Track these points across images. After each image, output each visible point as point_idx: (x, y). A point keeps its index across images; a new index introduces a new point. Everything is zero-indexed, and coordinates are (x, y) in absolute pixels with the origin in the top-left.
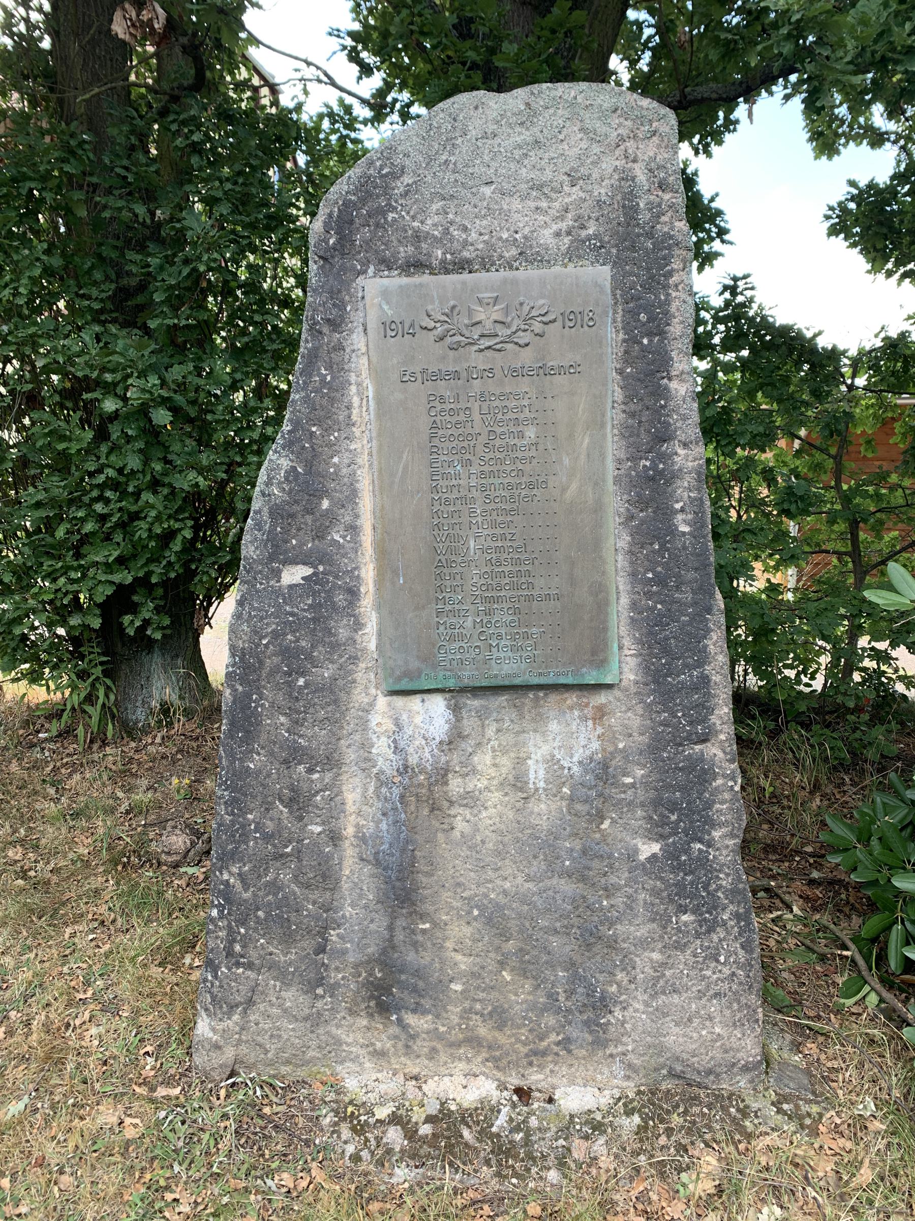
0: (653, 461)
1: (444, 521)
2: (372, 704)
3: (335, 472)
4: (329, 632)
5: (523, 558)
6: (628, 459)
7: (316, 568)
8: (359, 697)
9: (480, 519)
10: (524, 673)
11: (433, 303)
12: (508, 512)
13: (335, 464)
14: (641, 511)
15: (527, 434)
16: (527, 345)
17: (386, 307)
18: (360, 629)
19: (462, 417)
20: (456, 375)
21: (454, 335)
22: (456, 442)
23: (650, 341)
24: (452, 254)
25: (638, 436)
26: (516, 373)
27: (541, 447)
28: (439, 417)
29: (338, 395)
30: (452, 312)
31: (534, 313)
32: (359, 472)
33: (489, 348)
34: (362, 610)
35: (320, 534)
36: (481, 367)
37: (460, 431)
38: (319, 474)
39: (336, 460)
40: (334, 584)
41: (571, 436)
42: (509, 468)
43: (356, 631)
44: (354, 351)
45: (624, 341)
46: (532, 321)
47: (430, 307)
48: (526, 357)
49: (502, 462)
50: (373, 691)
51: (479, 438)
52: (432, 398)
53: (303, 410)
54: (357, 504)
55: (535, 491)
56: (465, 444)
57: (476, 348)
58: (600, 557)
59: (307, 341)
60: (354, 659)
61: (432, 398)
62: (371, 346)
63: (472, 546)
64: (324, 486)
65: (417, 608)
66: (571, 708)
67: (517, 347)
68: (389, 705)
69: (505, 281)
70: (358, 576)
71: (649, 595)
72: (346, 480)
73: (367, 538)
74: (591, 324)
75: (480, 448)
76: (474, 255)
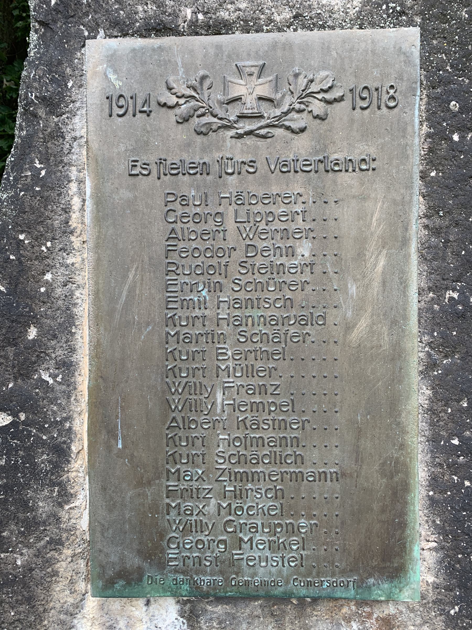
0: (462, 293)
1: (182, 365)
2: (78, 606)
3: (48, 294)
4: (25, 505)
5: (289, 420)
6: (430, 289)
7: (15, 415)
8: (61, 595)
9: (231, 364)
10: (287, 582)
11: (175, 71)
12: (269, 356)
13: (47, 282)
14: (446, 357)
15: (299, 251)
16: (302, 130)
17: (112, 77)
18: (67, 502)
19: (211, 226)
20: (205, 169)
21: (203, 115)
22: (202, 259)
23: (462, 138)
24: (205, 13)
25: (444, 259)
26: (285, 168)
27: (318, 269)
28: (179, 225)
29: (53, 195)
30: (201, 83)
31: (314, 88)
32: (77, 294)
33: (250, 133)
34: (72, 475)
35: (25, 370)
36: (239, 158)
37: (208, 244)
38: (27, 295)
39: (48, 277)
40: (38, 438)
41: (360, 256)
42: (272, 296)
43: (61, 505)
44: (75, 139)
45: (429, 135)
46: (310, 99)
47: (171, 79)
48: (301, 146)
49: (263, 287)
50: (82, 586)
51: (233, 254)
52: (171, 198)
53: (9, 212)
54: (73, 334)
55: (308, 329)
56: (214, 262)
57: (232, 132)
58: (398, 424)
59: (21, 129)
60: (57, 543)
61: (171, 198)
62: (91, 128)
63: (219, 400)
64: (31, 310)
65: (140, 484)
66: (348, 620)
67: (288, 134)
68: (102, 607)
69: (274, 45)
70: (70, 428)
71: (454, 468)
72: (60, 302)
73: (83, 380)
74: (392, 104)
75: (234, 268)
76: (234, 16)
